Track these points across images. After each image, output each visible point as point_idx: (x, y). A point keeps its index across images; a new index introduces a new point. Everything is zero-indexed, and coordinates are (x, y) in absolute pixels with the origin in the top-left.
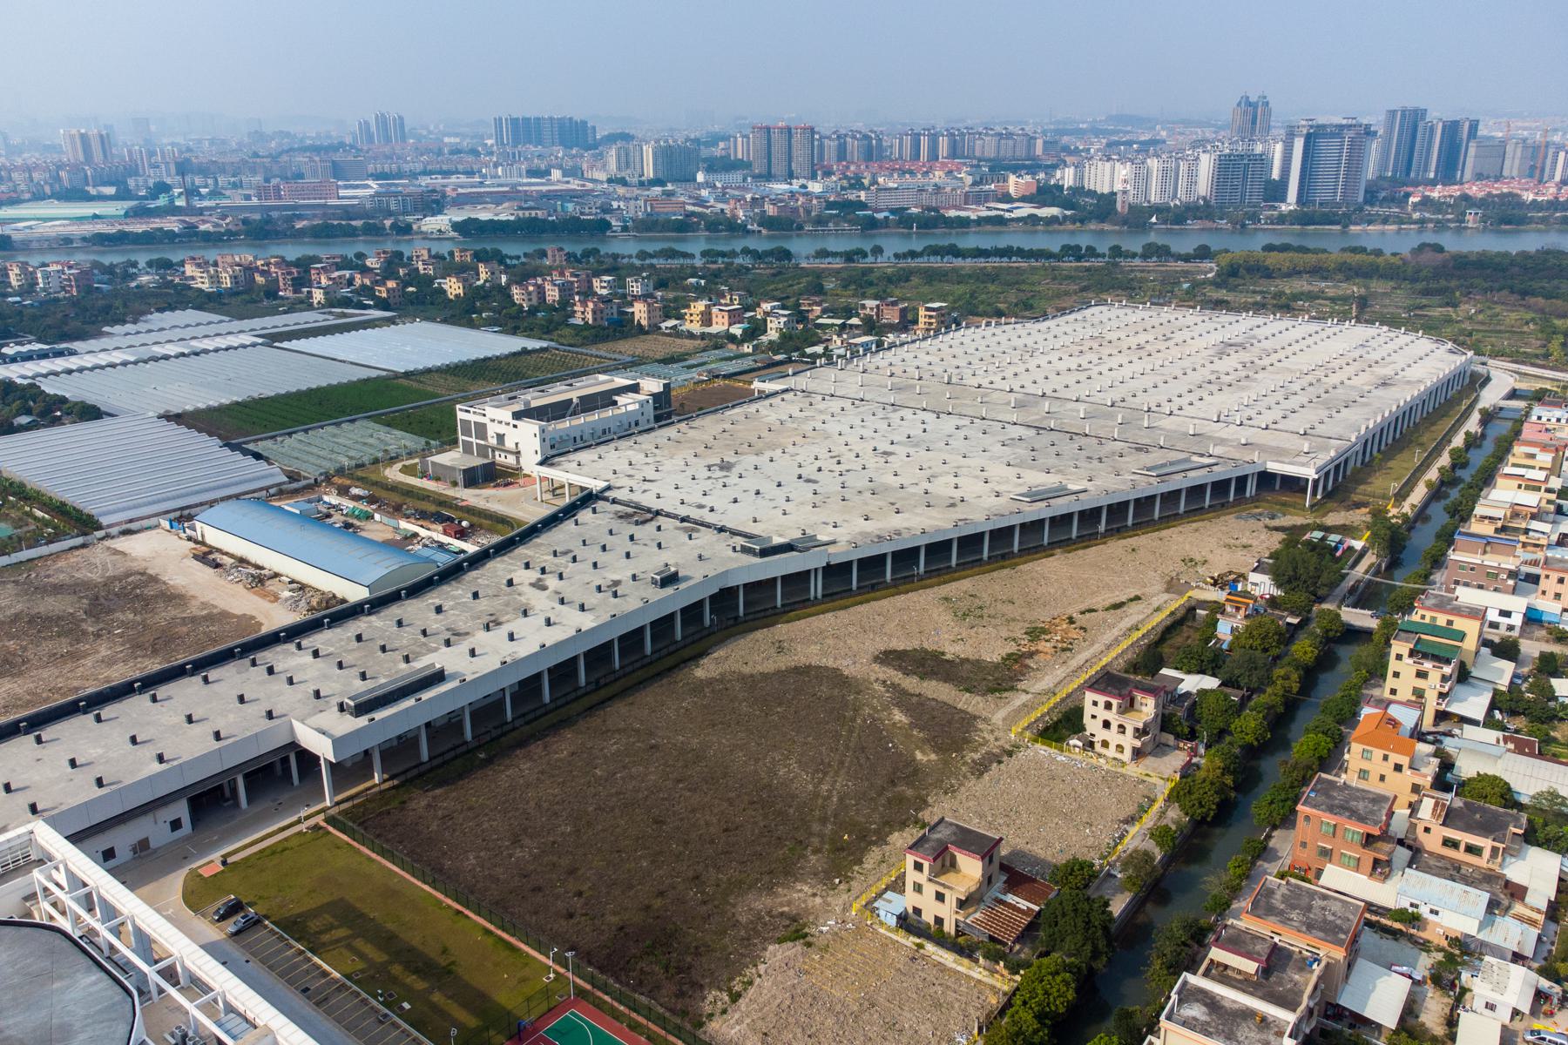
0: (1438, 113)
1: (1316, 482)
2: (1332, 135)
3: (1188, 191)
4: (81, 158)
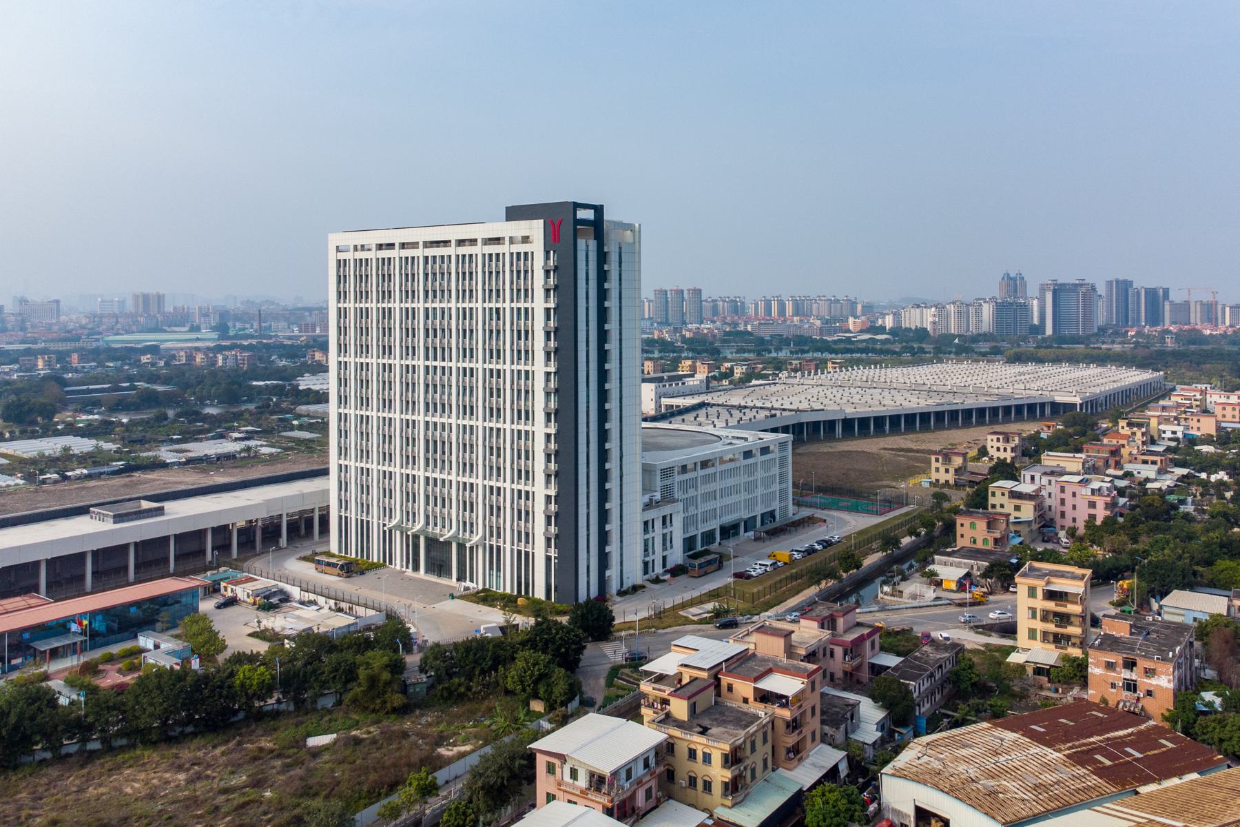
0: (1142, 281)
1: (1081, 405)
2: (1070, 291)
3: (977, 327)
4: (141, 309)
